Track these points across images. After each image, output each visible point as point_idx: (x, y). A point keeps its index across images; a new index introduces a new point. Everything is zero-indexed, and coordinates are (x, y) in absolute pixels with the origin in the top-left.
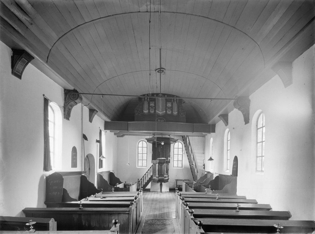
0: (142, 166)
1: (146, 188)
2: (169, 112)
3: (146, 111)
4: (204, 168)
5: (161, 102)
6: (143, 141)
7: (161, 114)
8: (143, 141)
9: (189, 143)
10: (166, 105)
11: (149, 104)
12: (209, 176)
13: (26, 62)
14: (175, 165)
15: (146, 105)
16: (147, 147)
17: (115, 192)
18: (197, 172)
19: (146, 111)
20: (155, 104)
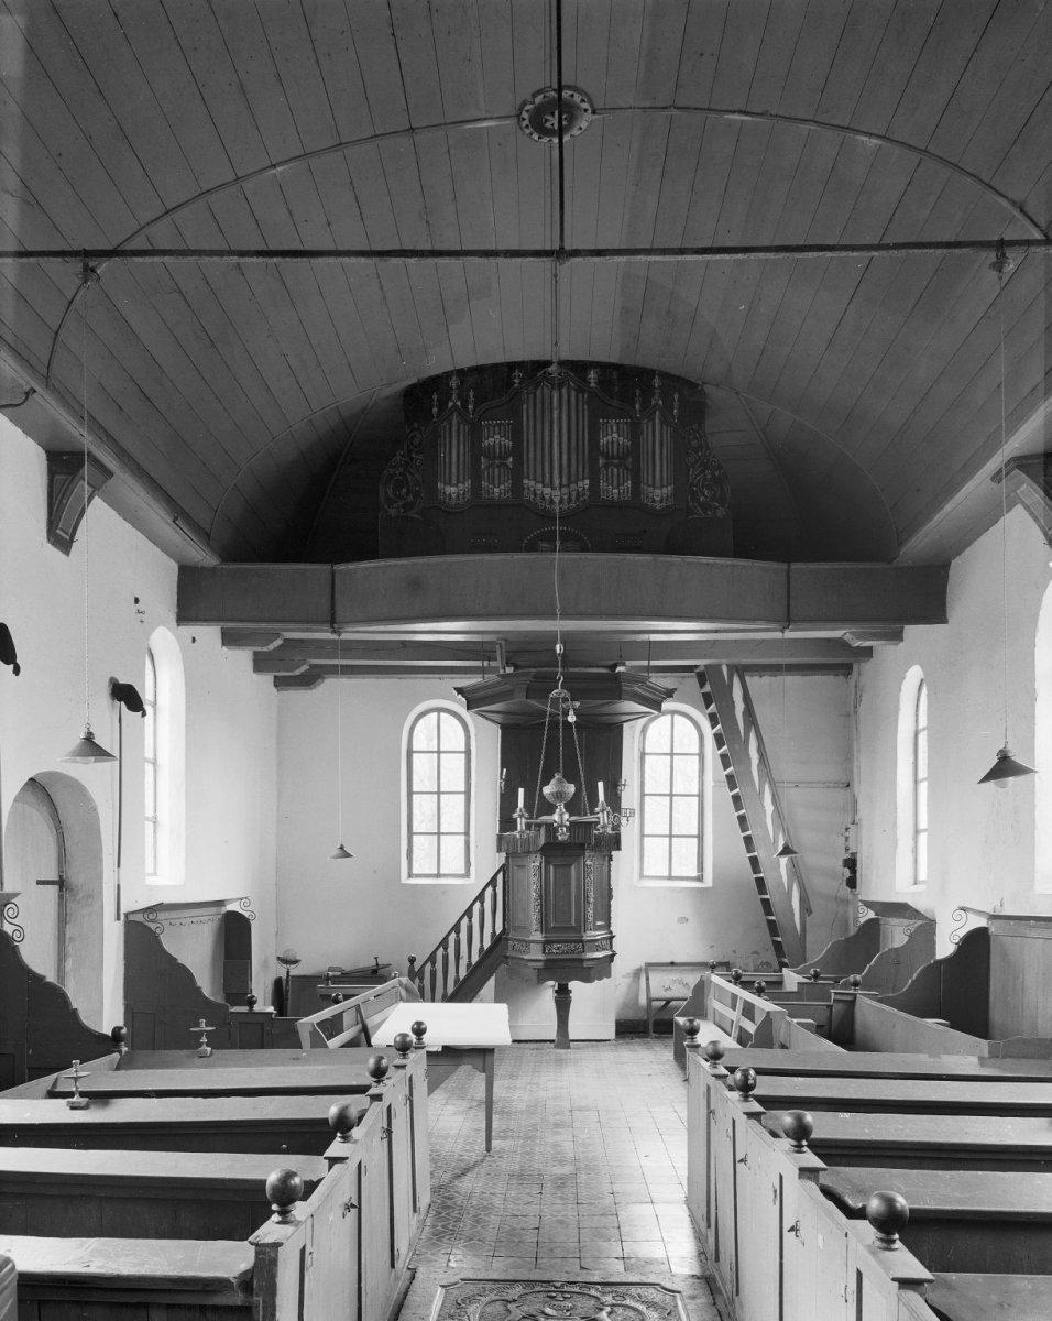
0: (438, 875)
3: (453, 490)
4: (852, 883)
6: (439, 710)
8: (439, 710)
9: (749, 711)
10: (594, 440)
11: (475, 433)
12: (897, 935)
14: (656, 864)
15: (454, 451)
17: (216, 1052)
18: (806, 909)
19: (453, 490)
20: (517, 434)
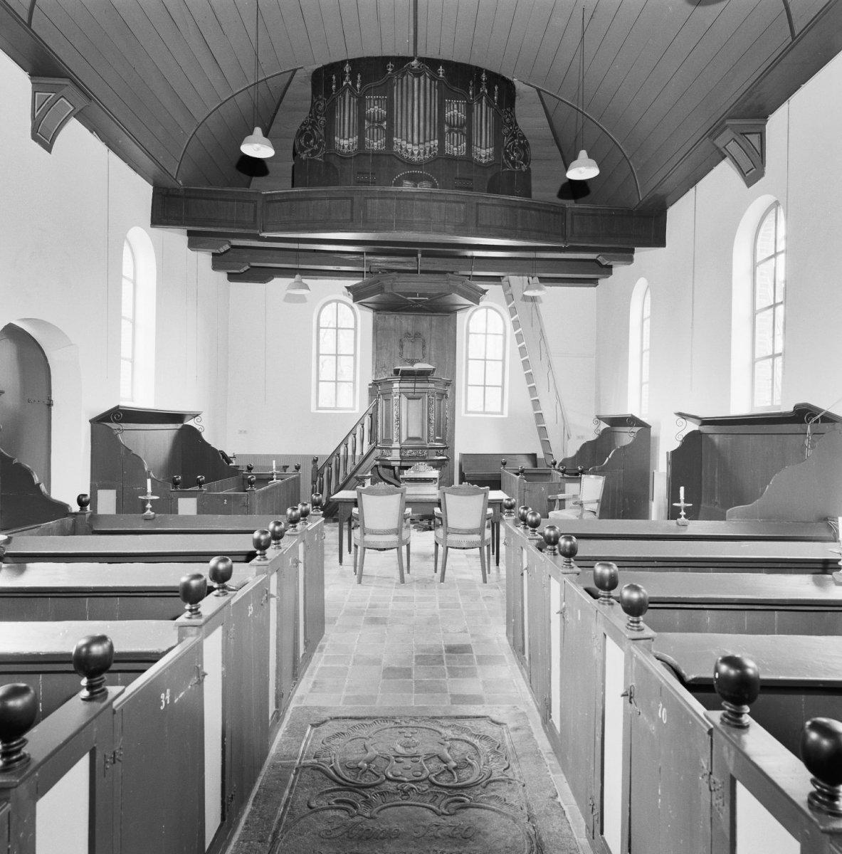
1: (220, 628)
2: (456, 148)
3: (346, 143)
5: (416, 95)
6: (338, 301)
7: (416, 152)
8: (338, 301)
11: (361, 104)
13: (70, 108)
16: (355, 329)
19: (346, 143)
20: (390, 109)
